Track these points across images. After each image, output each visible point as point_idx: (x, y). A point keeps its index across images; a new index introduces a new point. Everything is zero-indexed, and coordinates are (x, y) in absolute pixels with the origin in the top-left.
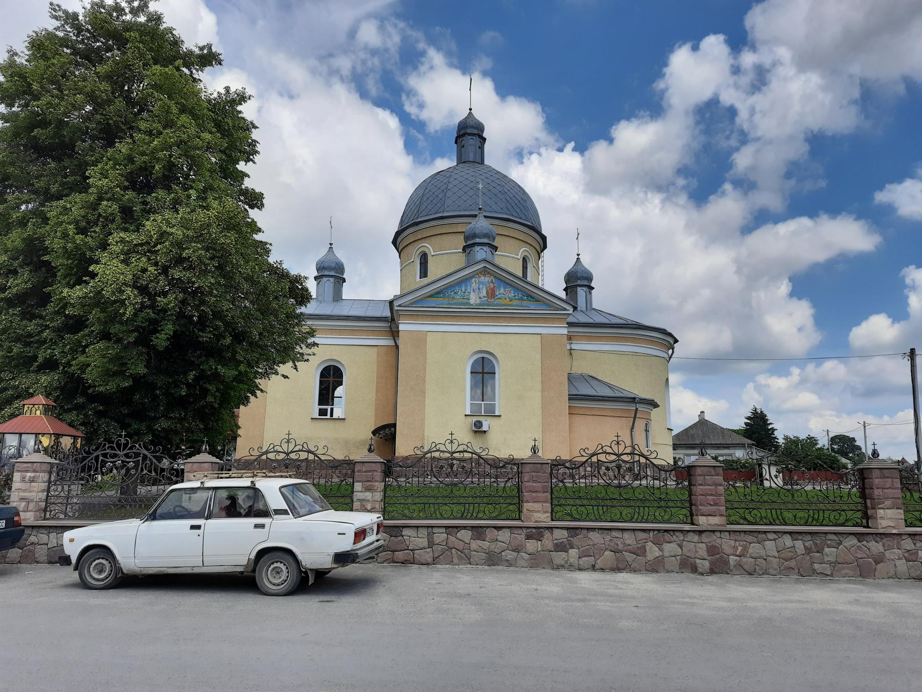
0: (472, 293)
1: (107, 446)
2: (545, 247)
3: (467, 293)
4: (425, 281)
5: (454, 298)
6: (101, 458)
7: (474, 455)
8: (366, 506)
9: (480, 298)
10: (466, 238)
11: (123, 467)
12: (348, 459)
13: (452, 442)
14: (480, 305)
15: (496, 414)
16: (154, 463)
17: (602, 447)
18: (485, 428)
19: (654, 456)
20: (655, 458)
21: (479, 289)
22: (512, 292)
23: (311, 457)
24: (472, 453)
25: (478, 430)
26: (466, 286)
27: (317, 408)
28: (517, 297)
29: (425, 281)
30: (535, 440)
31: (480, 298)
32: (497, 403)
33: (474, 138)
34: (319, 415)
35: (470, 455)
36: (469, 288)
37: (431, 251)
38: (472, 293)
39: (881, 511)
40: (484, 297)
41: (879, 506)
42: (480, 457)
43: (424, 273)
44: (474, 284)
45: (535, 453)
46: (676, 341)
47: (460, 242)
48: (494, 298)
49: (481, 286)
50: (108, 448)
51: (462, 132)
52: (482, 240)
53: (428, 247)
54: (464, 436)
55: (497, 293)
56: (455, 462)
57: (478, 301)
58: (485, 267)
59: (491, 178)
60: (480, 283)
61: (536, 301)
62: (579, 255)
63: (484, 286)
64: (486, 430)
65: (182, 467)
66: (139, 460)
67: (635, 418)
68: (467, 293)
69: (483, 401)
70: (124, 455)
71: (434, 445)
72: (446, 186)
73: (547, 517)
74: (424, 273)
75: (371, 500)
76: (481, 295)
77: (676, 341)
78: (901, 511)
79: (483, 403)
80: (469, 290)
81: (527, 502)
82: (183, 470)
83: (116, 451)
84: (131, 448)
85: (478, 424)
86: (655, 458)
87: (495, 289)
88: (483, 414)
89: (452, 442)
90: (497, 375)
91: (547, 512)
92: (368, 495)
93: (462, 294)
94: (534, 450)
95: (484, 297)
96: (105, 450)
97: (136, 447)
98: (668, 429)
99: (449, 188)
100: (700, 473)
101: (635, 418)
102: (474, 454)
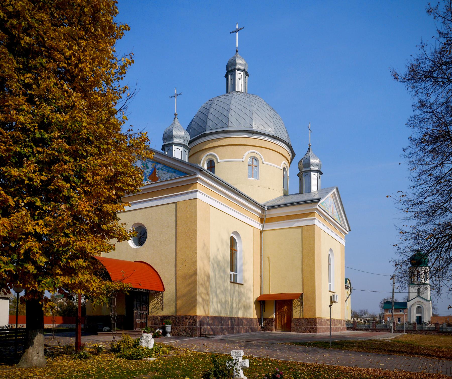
33: (242, 73)
51: (230, 69)
52: (315, 168)
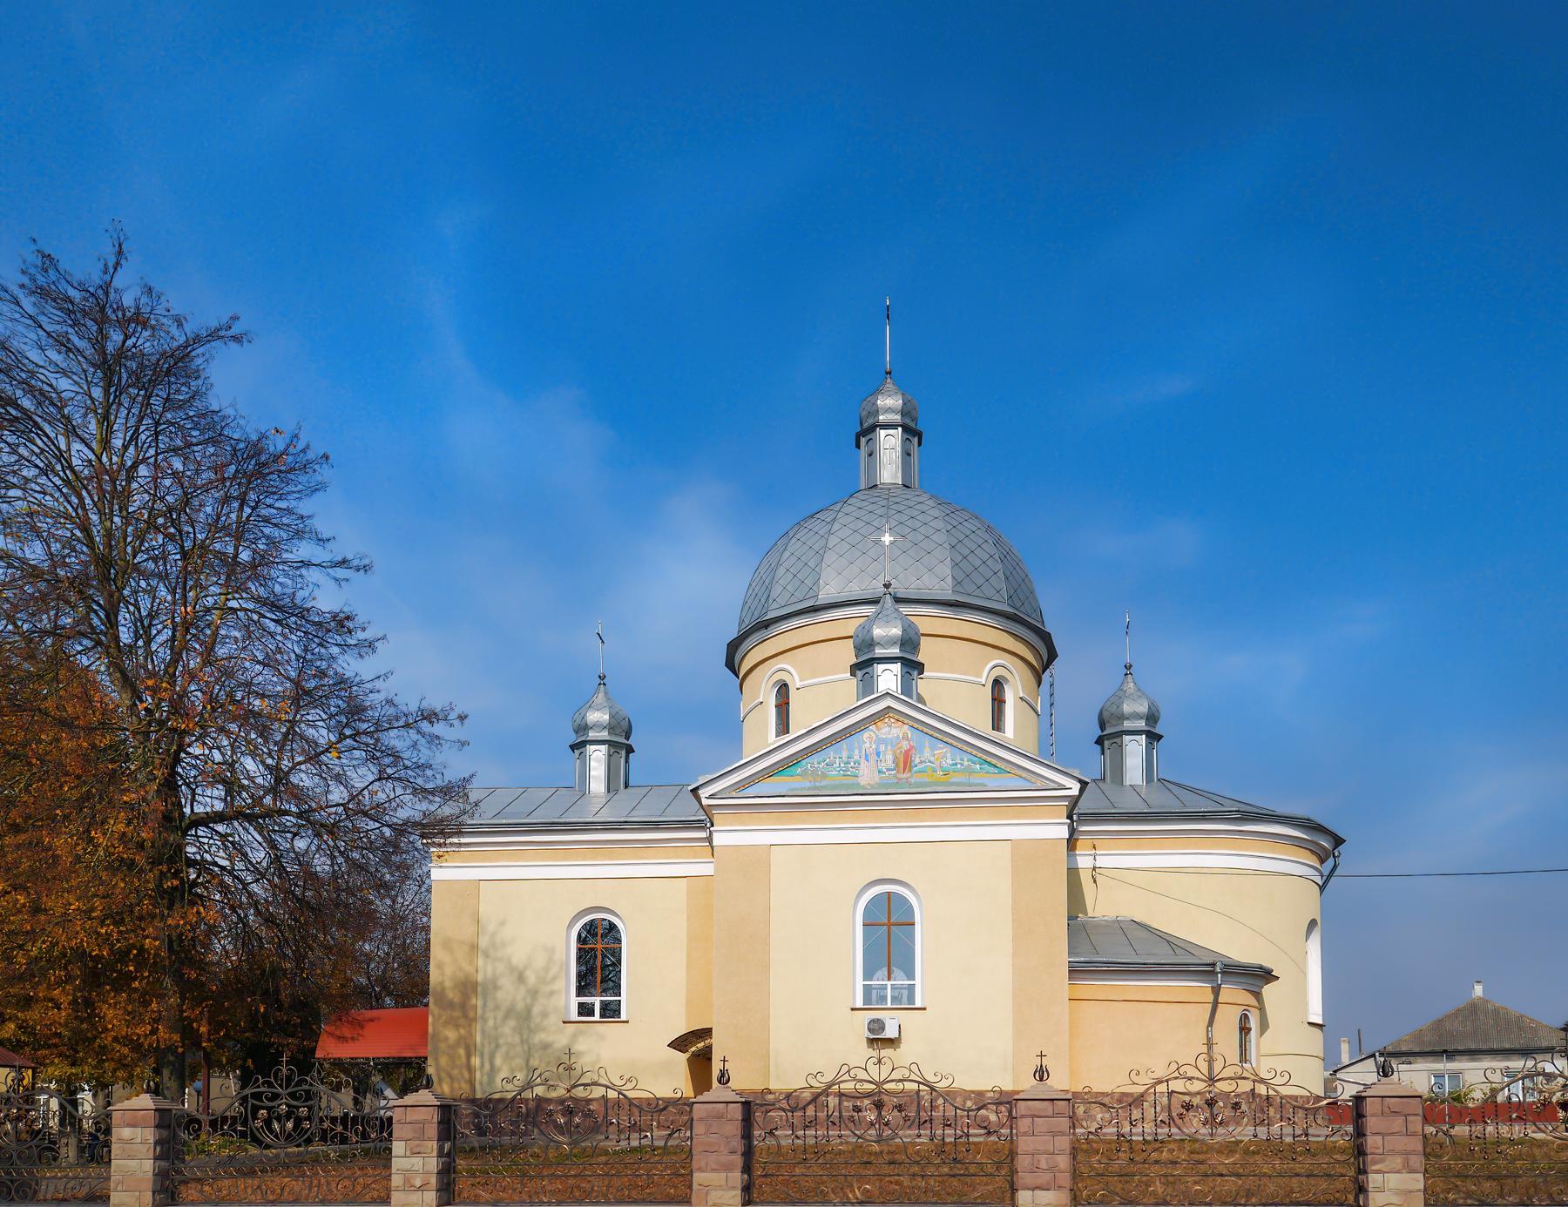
0: (864, 764)
1: (261, 1081)
2: (1052, 655)
3: (852, 764)
4: (787, 738)
5: (824, 775)
6: (251, 1101)
7: (922, 1087)
8: (412, 1181)
9: (880, 772)
10: (858, 649)
11: (288, 1116)
12: (679, 1095)
13: (880, 1061)
14: (881, 785)
15: (917, 1006)
16: (69, 1112)
17: (849, 1071)
18: (890, 1032)
19: (630, 1086)
20: (633, 1089)
21: (878, 754)
22: (949, 755)
23: (612, 1094)
24: (919, 1083)
25: (879, 1040)
26: (851, 750)
27: (574, 1001)
28: (959, 766)
29: (787, 738)
30: (724, 1061)
31: (880, 772)
32: (623, 998)
34: (580, 1014)
35: (914, 1086)
36: (857, 752)
37: (795, 682)
38: (864, 764)
39: (1379, 1177)
40: (888, 770)
41: (1374, 1168)
42: (933, 1089)
43: (783, 726)
44: (867, 745)
45: (1041, 1080)
46: (1338, 841)
47: (847, 654)
48: (910, 770)
49: (882, 748)
50: (263, 1084)
53: (791, 670)
54: (858, 1053)
55: (917, 761)
56: (885, 1098)
57: (877, 779)
58: (889, 707)
59: (921, 517)
60: (880, 741)
61: (999, 773)
62: (1131, 666)
63: (889, 747)
64: (892, 1037)
65: (389, 1114)
66: (253, 1104)
67: (1215, 1004)
68: (852, 764)
69: (889, 979)
70: (289, 1094)
71: (845, 1069)
72: (823, 542)
73: (733, 1197)
74: (783, 726)
75: (421, 1171)
76: (883, 766)
77: (1338, 841)
78: (1420, 1176)
79: (889, 983)
80: (856, 758)
81: (700, 1170)
82: (391, 1118)
83: (276, 1088)
84: (299, 1084)
85: (877, 1026)
86: (633, 1089)
87: (913, 751)
88: (889, 1005)
89: (880, 1061)
90: (918, 928)
91: (734, 1188)
92: (417, 1162)
93: (842, 765)
94: (1041, 1074)
95: (888, 770)
96: (259, 1087)
97: (307, 1081)
98: (1309, 1023)
99: (830, 545)
100: (1023, 1113)
101: (1215, 1004)
102: (923, 1084)
